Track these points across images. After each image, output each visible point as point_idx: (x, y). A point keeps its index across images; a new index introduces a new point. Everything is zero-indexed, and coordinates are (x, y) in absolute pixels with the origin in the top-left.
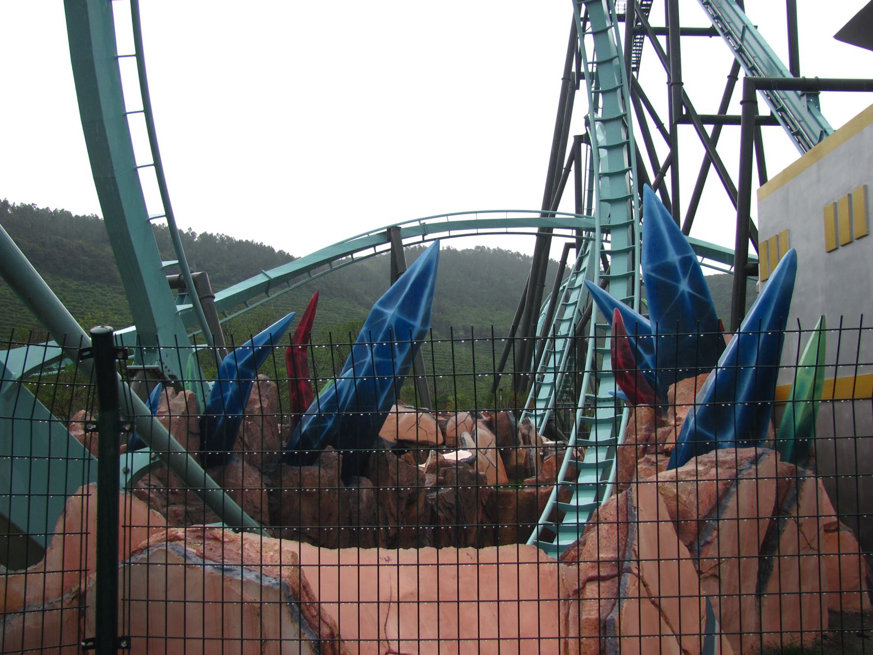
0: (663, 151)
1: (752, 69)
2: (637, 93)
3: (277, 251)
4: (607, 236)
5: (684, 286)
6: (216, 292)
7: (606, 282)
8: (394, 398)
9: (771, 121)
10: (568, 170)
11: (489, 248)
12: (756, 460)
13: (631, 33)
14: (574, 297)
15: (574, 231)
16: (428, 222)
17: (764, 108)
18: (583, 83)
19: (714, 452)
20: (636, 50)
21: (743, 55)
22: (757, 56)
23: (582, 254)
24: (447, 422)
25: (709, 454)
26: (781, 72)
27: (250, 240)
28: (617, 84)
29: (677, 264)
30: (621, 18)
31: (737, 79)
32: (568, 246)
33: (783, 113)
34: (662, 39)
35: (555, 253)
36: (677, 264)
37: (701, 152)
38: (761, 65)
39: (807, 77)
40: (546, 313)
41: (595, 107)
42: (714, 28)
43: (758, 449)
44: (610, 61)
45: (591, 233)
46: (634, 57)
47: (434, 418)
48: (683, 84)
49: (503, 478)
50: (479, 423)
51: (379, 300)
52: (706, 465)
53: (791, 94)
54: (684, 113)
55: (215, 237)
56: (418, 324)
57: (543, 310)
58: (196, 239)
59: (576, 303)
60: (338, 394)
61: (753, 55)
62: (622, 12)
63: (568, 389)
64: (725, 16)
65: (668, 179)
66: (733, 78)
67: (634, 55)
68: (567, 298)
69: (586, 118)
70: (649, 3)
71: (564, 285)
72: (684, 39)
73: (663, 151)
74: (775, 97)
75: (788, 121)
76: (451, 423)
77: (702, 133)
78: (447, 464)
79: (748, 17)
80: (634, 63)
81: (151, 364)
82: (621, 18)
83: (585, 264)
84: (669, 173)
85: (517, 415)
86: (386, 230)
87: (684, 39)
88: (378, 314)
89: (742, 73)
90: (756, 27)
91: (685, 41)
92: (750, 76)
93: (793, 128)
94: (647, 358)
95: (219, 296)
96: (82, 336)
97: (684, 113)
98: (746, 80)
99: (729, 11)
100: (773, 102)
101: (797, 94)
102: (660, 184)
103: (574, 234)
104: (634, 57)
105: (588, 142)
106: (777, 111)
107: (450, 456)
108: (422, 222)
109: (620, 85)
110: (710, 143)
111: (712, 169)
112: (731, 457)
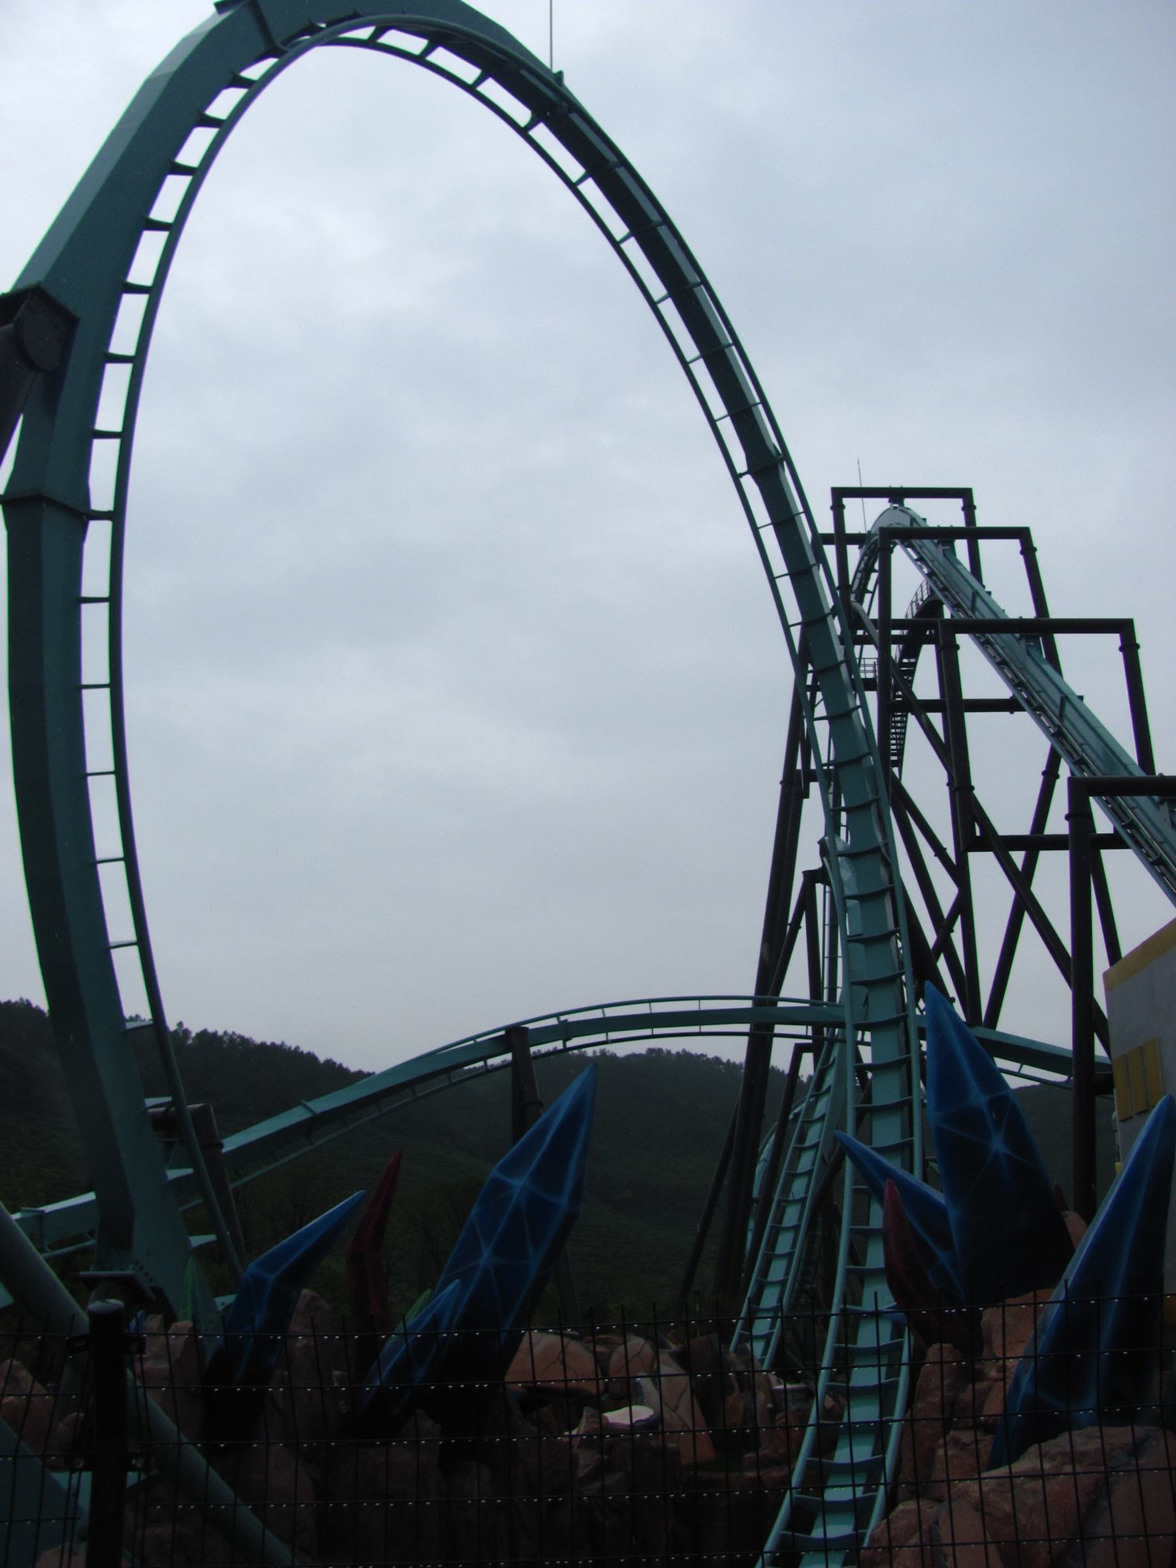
0: (946, 892)
1: (1078, 763)
2: (904, 804)
3: (322, 1059)
4: (863, 1034)
5: (998, 1145)
6: (225, 1137)
7: (866, 1113)
8: (526, 1321)
9: (1114, 841)
10: (796, 926)
11: (669, 1052)
12: (1136, 1449)
13: (887, 710)
14: (814, 1135)
15: (810, 1028)
16: (572, 1018)
17: (1103, 824)
18: (815, 787)
19: (1066, 1436)
20: (896, 733)
21: (1065, 743)
22: (1087, 743)
23: (823, 1064)
24: (610, 1355)
25: (1059, 1439)
26: (1125, 767)
27: (278, 1042)
28: (871, 797)
29: (985, 1109)
30: (869, 685)
31: (1057, 777)
32: (799, 1051)
33: (1134, 831)
34: (936, 719)
35: (781, 1055)
36: (985, 1109)
37: (1006, 894)
38: (1094, 757)
39: (1166, 774)
40: (768, 1159)
41: (833, 826)
42: (1016, 699)
43: (1136, 1428)
44: (858, 760)
45: (837, 1030)
46: (893, 745)
47: (587, 1348)
48: (972, 788)
49: (706, 1451)
50: (664, 1356)
51: (501, 1162)
52: (1055, 1460)
53: (1143, 800)
54: (978, 833)
55: (221, 1037)
56: (564, 1201)
57: (761, 1153)
58: (190, 1042)
59: (816, 1146)
60: (436, 1320)
61: (1081, 741)
62: (870, 676)
63: (808, 1286)
64: (1033, 683)
65: (957, 937)
66: (1050, 775)
67: (893, 742)
68: (802, 1138)
69: (822, 843)
70: (913, 660)
71: (796, 1111)
72: (971, 718)
73: (946, 892)
74: (1120, 805)
75: (1143, 842)
76: (616, 1357)
77: (1007, 865)
78: (614, 1430)
79: (1067, 683)
80: (894, 755)
81: (123, 1270)
82: (869, 685)
83: (830, 1080)
84: (958, 926)
85: (726, 1338)
86: (503, 1033)
87: (971, 718)
88: (499, 1187)
89: (1064, 770)
90: (1081, 698)
91: (972, 720)
92: (1078, 775)
93: (1151, 853)
94: (943, 1256)
95: (231, 1144)
96: (73, 1316)
97: (978, 833)
98: (1072, 782)
99: (1035, 672)
100: (1116, 813)
101: (1153, 801)
102: (945, 944)
103: (810, 1033)
104: (893, 745)
105: (826, 882)
106: (1124, 827)
107: (618, 1417)
108: (562, 1018)
109: (876, 797)
110: (1021, 880)
111: (1027, 923)
112: (1093, 1445)
